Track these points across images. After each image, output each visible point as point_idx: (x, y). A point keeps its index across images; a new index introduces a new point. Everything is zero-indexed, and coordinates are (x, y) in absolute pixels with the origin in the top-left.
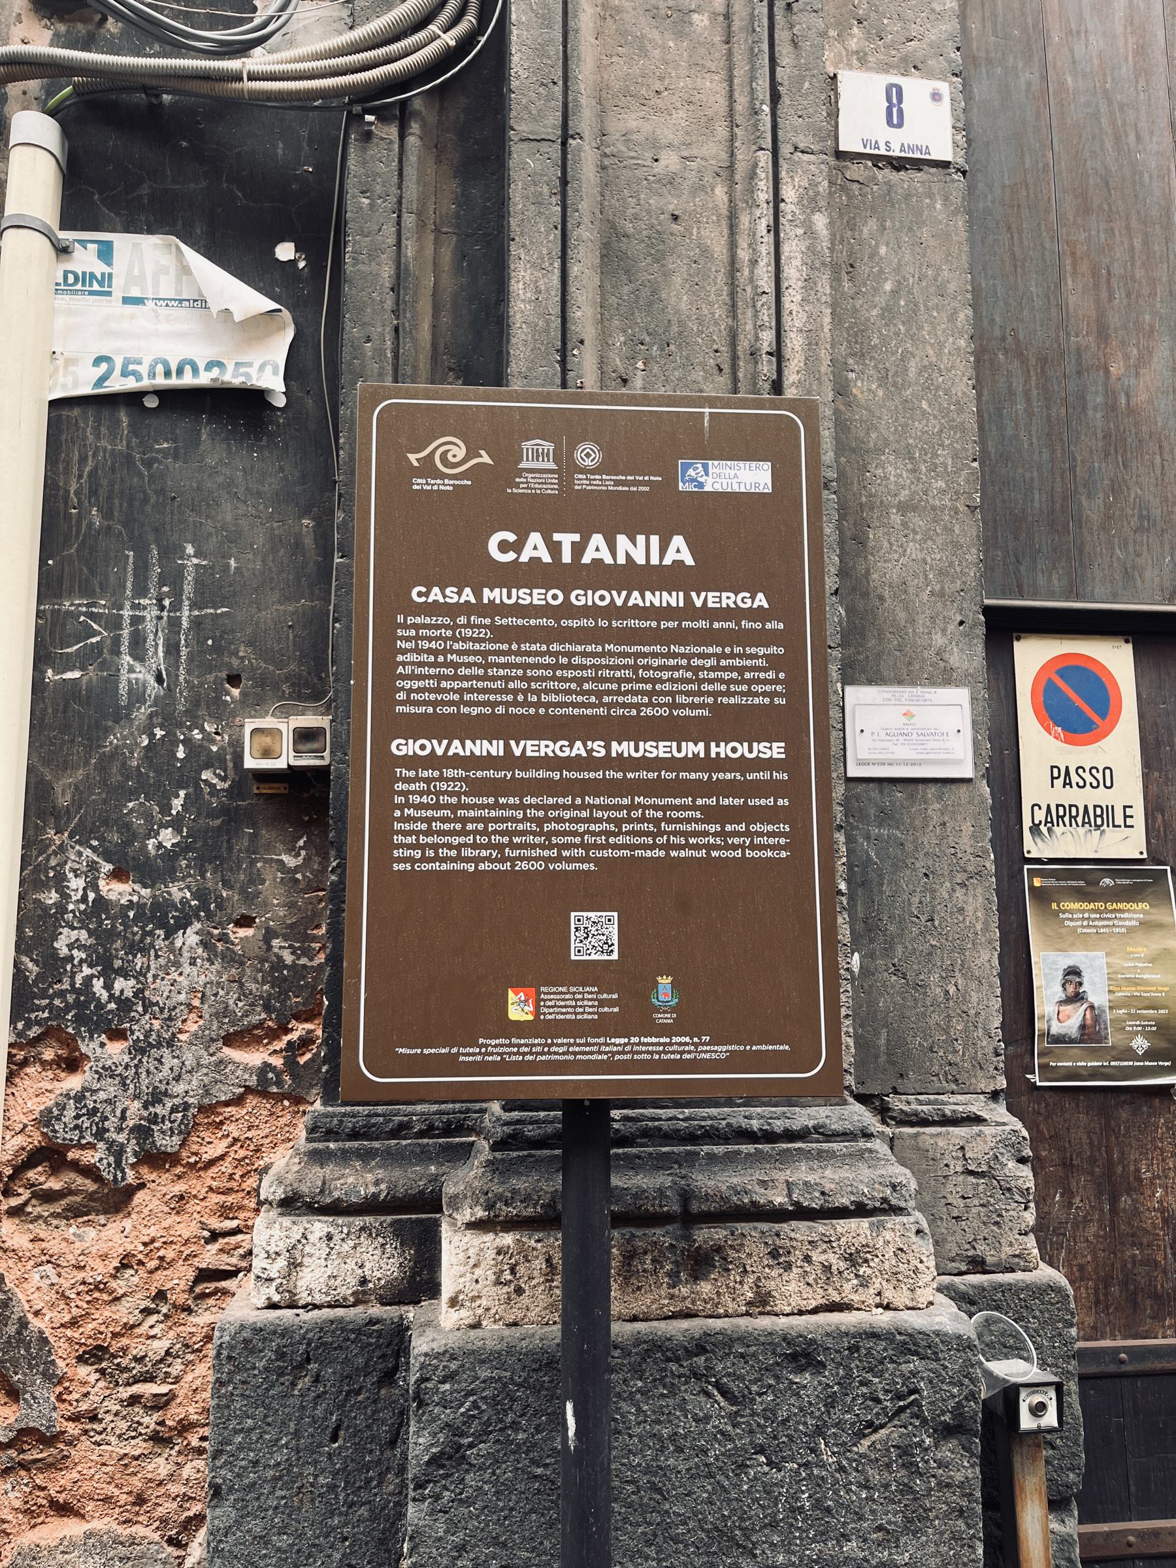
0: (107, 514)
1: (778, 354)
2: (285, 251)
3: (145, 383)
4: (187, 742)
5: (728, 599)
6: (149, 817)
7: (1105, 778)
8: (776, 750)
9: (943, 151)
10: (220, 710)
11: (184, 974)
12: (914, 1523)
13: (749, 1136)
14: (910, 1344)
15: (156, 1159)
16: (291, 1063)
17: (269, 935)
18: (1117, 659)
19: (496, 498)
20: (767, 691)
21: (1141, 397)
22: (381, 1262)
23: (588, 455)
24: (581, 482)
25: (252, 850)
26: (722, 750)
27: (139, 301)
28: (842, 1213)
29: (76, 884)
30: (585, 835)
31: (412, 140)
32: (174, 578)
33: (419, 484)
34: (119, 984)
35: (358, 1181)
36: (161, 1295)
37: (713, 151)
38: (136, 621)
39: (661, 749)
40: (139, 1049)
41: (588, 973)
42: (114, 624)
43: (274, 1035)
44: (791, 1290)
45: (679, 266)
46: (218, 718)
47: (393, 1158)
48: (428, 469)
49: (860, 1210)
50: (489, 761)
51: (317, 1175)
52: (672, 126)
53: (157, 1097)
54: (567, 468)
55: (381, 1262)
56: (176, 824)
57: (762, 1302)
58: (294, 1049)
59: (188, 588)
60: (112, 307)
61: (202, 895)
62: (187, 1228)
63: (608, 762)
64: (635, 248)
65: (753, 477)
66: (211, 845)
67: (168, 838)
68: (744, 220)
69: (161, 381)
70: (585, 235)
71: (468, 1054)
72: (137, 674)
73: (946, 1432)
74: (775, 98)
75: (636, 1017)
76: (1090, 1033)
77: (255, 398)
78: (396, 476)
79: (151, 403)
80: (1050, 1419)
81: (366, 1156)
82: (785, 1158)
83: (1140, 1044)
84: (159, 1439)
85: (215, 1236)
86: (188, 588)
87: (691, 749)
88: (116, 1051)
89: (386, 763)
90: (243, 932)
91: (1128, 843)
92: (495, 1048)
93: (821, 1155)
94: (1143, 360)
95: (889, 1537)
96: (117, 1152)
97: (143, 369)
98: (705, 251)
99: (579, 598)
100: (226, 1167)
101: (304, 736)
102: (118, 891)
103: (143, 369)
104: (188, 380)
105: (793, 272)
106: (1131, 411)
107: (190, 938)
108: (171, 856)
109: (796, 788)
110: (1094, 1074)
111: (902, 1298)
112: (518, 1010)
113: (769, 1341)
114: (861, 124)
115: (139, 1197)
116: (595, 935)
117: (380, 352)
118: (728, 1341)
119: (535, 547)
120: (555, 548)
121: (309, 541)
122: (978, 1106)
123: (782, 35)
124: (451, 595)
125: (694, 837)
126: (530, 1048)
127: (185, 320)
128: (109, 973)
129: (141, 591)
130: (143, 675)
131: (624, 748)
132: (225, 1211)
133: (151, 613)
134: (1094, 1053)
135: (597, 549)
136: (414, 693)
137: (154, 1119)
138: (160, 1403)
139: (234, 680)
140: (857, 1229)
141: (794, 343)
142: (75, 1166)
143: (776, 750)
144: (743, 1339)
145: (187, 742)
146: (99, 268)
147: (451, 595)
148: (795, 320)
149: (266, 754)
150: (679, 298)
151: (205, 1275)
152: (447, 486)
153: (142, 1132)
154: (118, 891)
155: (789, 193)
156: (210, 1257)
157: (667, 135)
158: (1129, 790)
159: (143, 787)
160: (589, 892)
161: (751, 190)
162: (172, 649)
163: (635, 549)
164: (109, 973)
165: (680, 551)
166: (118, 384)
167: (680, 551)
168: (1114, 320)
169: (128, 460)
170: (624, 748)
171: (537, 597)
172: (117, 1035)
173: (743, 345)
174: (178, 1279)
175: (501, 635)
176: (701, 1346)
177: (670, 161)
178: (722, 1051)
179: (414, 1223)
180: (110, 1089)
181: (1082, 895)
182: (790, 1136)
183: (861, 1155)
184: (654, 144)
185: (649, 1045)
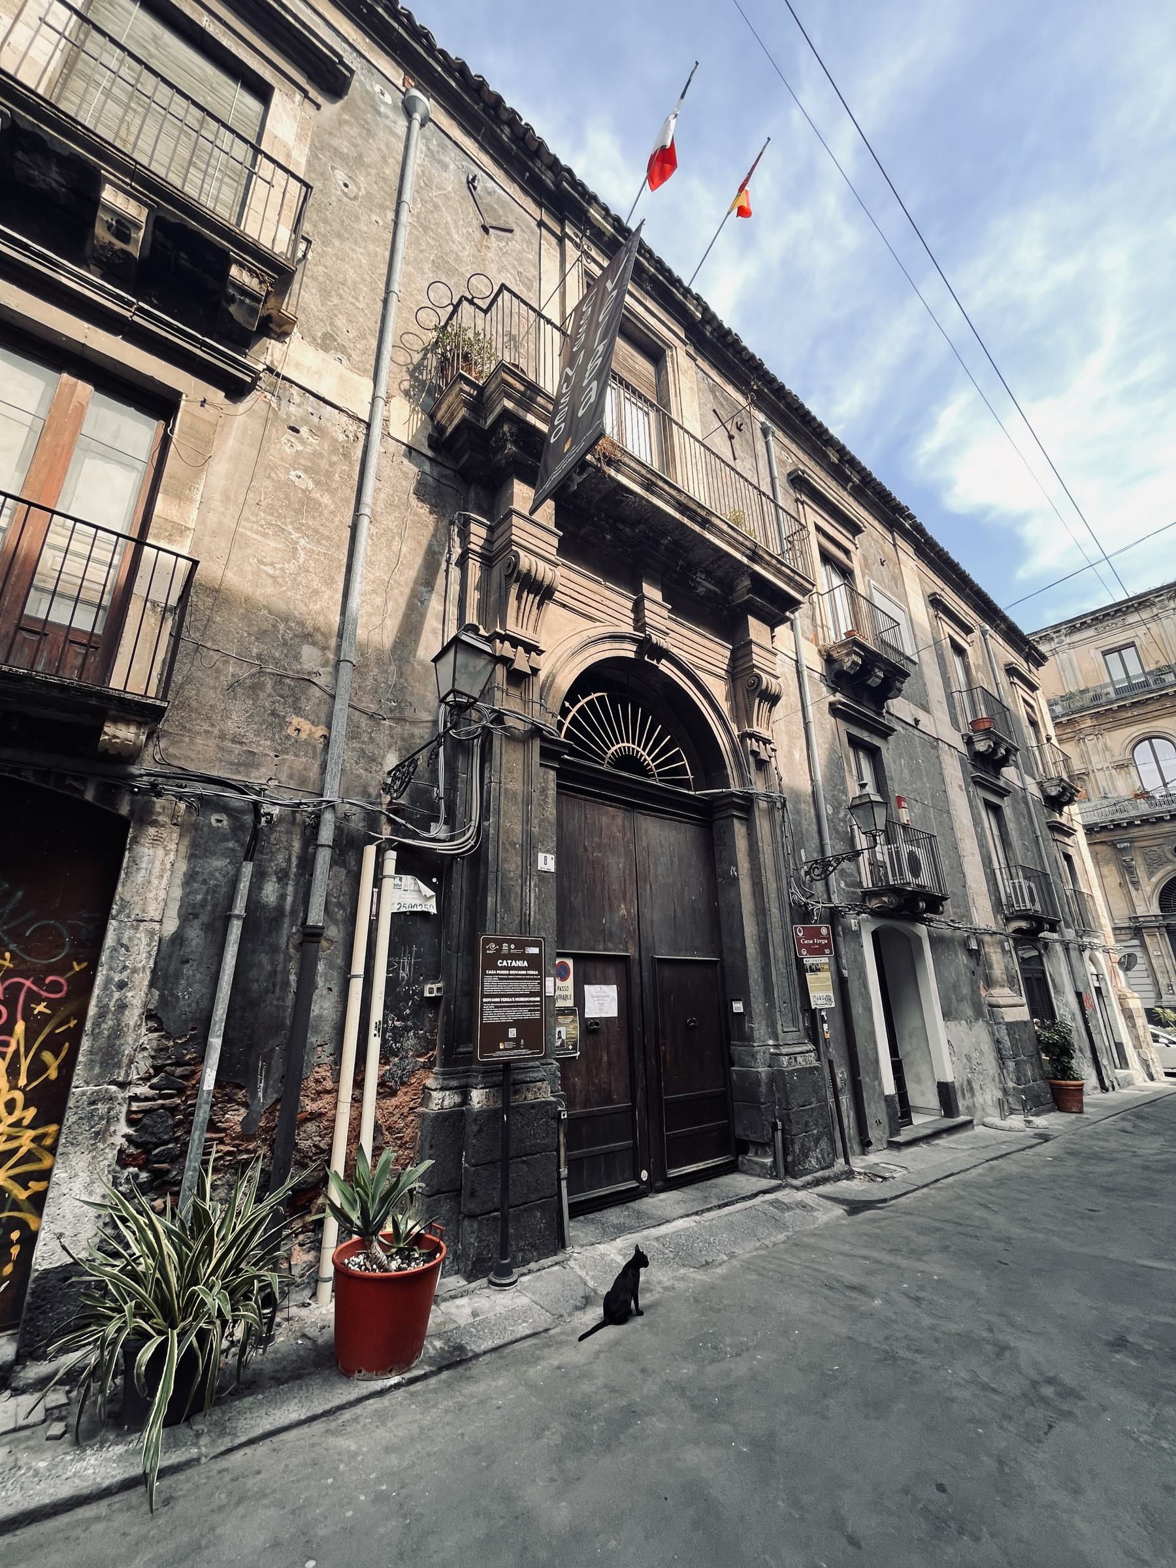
7: (567, 989)
10: (418, 983)
12: (548, 1135)
15: (403, 1084)
18: (570, 963)
20: (537, 989)
23: (513, 946)
30: (513, 1015)
32: (411, 953)
35: (454, 1083)
37: (519, 872)
39: (522, 999)
42: (399, 963)
44: (530, 1096)
47: (457, 1078)
53: (404, 1069)
54: (510, 949)
57: (525, 1098)
60: (402, 892)
65: (535, 950)
66: (416, 1013)
67: (408, 1011)
75: (518, 1047)
76: (562, 1044)
84: (400, 1147)
91: (570, 1003)
92: (498, 1053)
101: (438, 989)
104: (415, 909)
109: (541, 1006)
112: (501, 1047)
114: (541, 865)
116: (512, 1033)
119: (505, 963)
125: (526, 1014)
127: (415, 895)
135: (514, 964)
136: (487, 990)
138: (401, 1138)
153: (401, 1078)
158: (571, 992)
160: (511, 1025)
165: (526, 964)
167: (526, 964)
174: (406, 1110)
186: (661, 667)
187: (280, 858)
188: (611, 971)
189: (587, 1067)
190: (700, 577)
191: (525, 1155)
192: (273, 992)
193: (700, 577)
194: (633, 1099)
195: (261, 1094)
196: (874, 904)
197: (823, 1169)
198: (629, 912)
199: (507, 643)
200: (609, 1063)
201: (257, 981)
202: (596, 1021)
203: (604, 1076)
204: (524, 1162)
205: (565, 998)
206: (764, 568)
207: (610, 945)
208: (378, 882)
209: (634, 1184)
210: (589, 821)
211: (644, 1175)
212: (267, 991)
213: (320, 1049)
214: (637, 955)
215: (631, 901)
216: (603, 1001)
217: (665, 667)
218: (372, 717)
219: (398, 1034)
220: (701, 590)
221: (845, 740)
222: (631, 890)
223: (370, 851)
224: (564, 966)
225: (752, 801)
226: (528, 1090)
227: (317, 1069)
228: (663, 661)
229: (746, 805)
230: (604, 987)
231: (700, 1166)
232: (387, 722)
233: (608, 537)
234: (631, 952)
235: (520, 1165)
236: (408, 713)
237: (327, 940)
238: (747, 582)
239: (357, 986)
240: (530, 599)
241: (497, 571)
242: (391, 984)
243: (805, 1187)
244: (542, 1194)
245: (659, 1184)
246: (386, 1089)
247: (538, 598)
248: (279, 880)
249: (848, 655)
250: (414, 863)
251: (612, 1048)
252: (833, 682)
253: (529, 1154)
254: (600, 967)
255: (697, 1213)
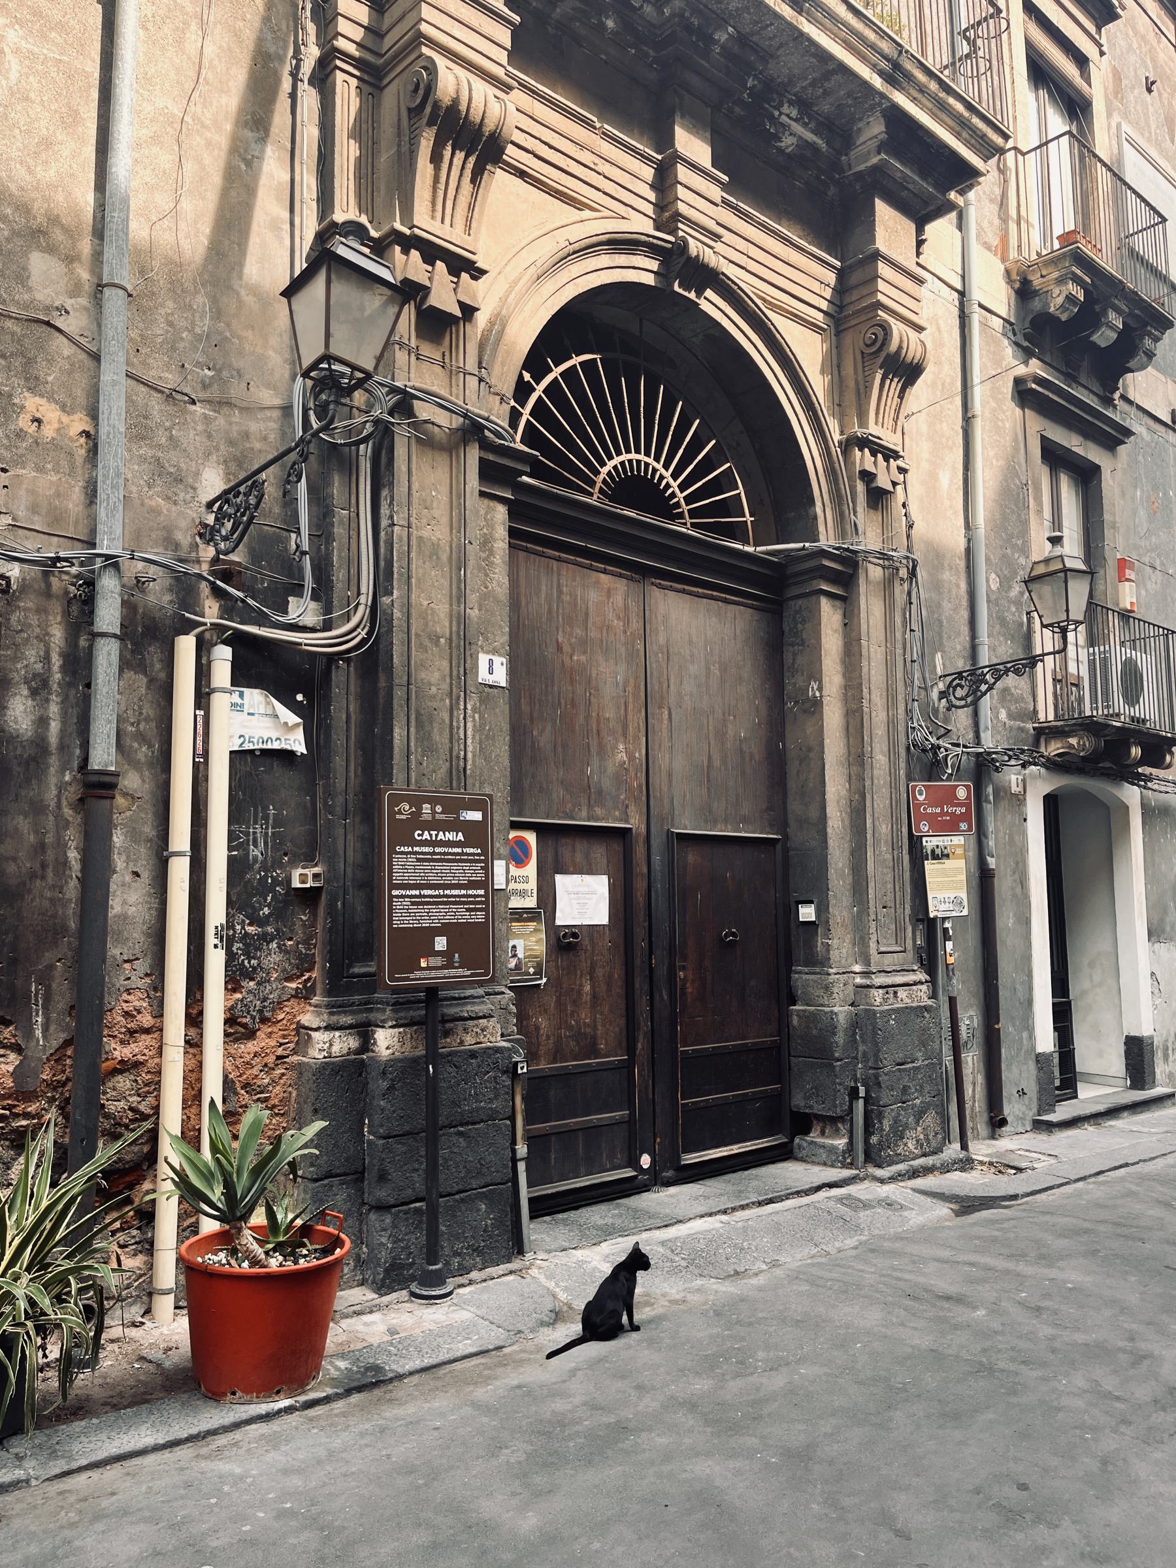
0: (244, 794)
1: (465, 759)
2: (300, 697)
3: (256, 747)
4: (272, 877)
5: (472, 850)
6: (260, 904)
7: (526, 880)
8: (482, 892)
9: (503, 684)
10: (281, 865)
11: (272, 958)
12: (496, 1097)
13: (455, 999)
14: (498, 1050)
15: (264, 1020)
16: (305, 986)
17: (298, 943)
18: (531, 838)
19: (416, 822)
20: (480, 876)
21: (542, 744)
22: (353, 1043)
23: (439, 809)
24: (438, 817)
25: (292, 914)
26: (470, 892)
27: (252, 714)
28: (481, 1018)
29: (238, 927)
31: (352, 669)
32: (266, 817)
33: (398, 817)
34: (253, 962)
35: (347, 1020)
36: (266, 1065)
38: (255, 833)
40: (259, 984)
41: (439, 953)
43: (298, 977)
44: (469, 1039)
45: (435, 725)
46: (280, 868)
47: (352, 1013)
48: (400, 812)
49: (484, 1017)
50: (416, 897)
51: (334, 1018)
52: (435, 677)
53: (265, 999)
54: (434, 812)
55: (353, 1043)
56: (269, 906)
57: (462, 1043)
58: (306, 981)
59: (271, 821)
61: (277, 930)
62: (273, 1043)
63: (444, 896)
64: (424, 718)
65: (477, 816)
66: (280, 913)
67: (266, 910)
68: (455, 713)
69: (261, 746)
70: (413, 717)
71: (412, 976)
72: (255, 852)
73: (504, 1072)
74: (465, 673)
75: (449, 965)
77: (291, 753)
78: (392, 814)
79: (258, 753)
80: (525, 1070)
81: (345, 1012)
82: (465, 1004)
83: (532, 970)
85: (281, 1044)
86: (271, 821)
87: (463, 892)
88: (252, 984)
89: (391, 897)
90: (290, 943)
91: (531, 902)
92: (418, 974)
93: (473, 1003)
94: (543, 731)
95: (491, 1101)
96: (253, 1018)
97: (255, 741)
98: (443, 721)
99: (438, 850)
100: (284, 1022)
101: (316, 876)
102: (250, 929)
103: (255, 741)
105: (469, 733)
106: (539, 748)
107: (274, 945)
108: (268, 917)
109: (486, 903)
110: (519, 981)
111: (493, 1040)
112: (423, 964)
113: (465, 1051)
114: (483, 675)
115: (258, 1033)
116: (441, 943)
117: (342, 744)
118: (456, 1052)
119: (426, 836)
120: (431, 835)
121: (309, 805)
122: (503, 989)
123: (468, 653)
124: (406, 849)
126: (425, 974)
127: (268, 722)
128: (249, 958)
129: (256, 823)
130: (256, 852)
131: (447, 892)
132: (284, 1037)
133: (259, 831)
134: (518, 974)
135: (441, 836)
136: (398, 878)
137: (264, 1007)
139: (286, 854)
140: (483, 1022)
141: (470, 755)
142: (240, 1024)
143: (482, 892)
144: (460, 1051)
145: (272, 877)
146: (239, 701)
147: (406, 849)
148: (470, 749)
149: (303, 882)
150: (436, 737)
151: (279, 1058)
152: (404, 817)
153: (260, 1012)
154: (250, 929)
155: (469, 707)
156: (280, 1051)
157: (433, 681)
158: (532, 885)
159: (258, 893)
160: (439, 931)
161: (458, 704)
162: (266, 843)
163: (450, 836)
164: (249, 958)
165: (460, 837)
166: (248, 746)
167: (460, 837)
168: (535, 715)
169: (251, 775)
170: (447, 892)
171: (426, 849)
172: (252, 979)
173: (454, 754)
174: (271, 1059)
175: (418, 860)
176: (450, 1054)
177: (434, 689)
178: (469, 973)
179: (364, 1032)
180: (251, 998)
181: (518, 921)
182: (465, 998)
183: (482, 1002)
184: (430, 684)
185: (453, 972)
186: (705, 306)
187: (32, 655)
188: (599, 852)
189: (558, 1002)
190: (788, 113)
191: (462, 1125)
192: (43, 878)
193: (788, 113)
194: (631, 1049)
195: (39, 1033)
196: (1053, 748)
197: (925, 1155)
198: (631, 758)
199: (415, 254)
200: (594, 996)
201: (14, 859)
202: (574, 932)
203: (585, 1016)
204: (460, 1134)
205: (523, 894)
206: (914, 100)
207: (598, 811)
208: (203, 698)
209: (629, 1173)
210: (566, 598)
211: (646, 1161)
212: (33, 876)
213: (127, 966)
214: (643, 828)
215: (636, 738)
216: (585, 900)
217: (712, 304)
218: (170, 396)
219: (252, 945)
220: (788, 142)
221: (1036, 451)
222: (636, 719)
223: (186, 646)
224: (522, 843)
225: (854, 565)
226: (466, 1030)
227: (125, 996)
228: (709, 293)
229: (844, 573)
230: (588, 878)
231: (735, 1149)
232: (198, 408)
233: (610, 24)
234: (635, 822)
235: (454, 1139)
236: (236, 391)
237: (125, 795)
238: (876, 128)
239: (180, 870)
240: (457, 161)
241: (393, 97)
242: (236, 868)
243: (893, 1179)
244: (488, 1179)
245: (669, 1174)
246: (237, 1028)
247: (472, 160)
248: (34, 693)
249: (1061, 281)
250: (260, 665)
251: (600, 973)
252: (1026, 337)
253: (467, 1124)
254: (581, 846)
255: (725, 1212)
